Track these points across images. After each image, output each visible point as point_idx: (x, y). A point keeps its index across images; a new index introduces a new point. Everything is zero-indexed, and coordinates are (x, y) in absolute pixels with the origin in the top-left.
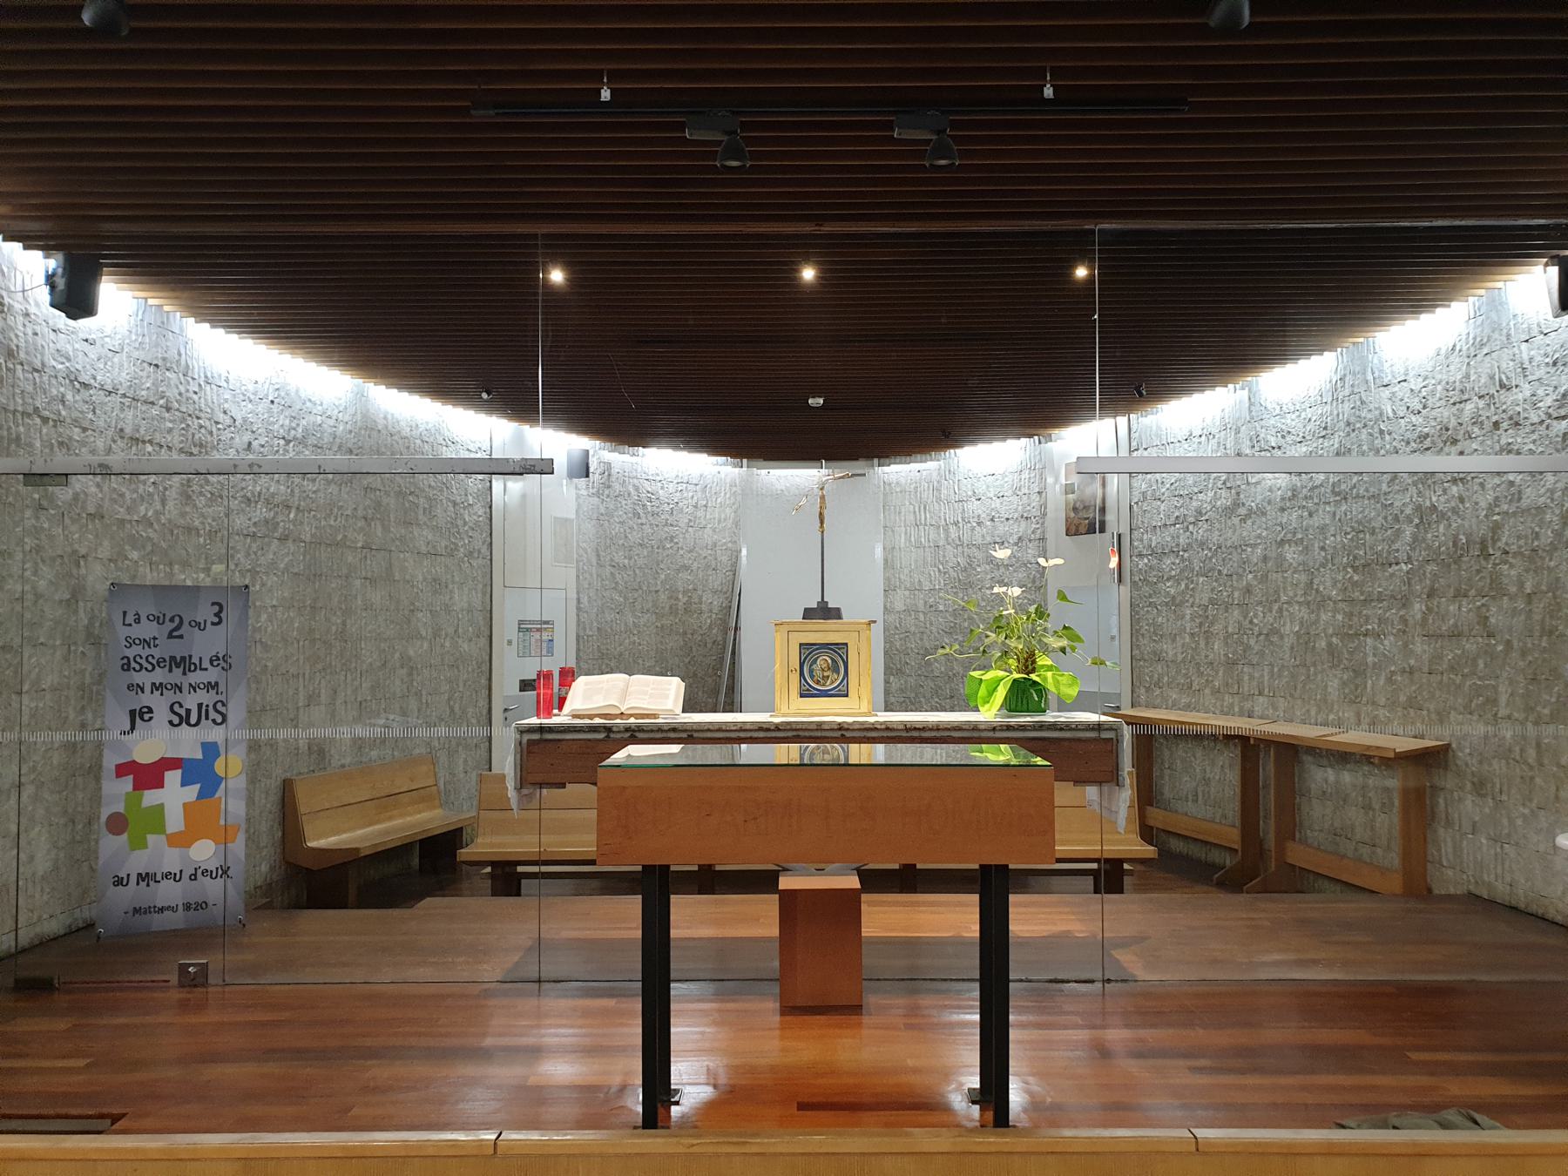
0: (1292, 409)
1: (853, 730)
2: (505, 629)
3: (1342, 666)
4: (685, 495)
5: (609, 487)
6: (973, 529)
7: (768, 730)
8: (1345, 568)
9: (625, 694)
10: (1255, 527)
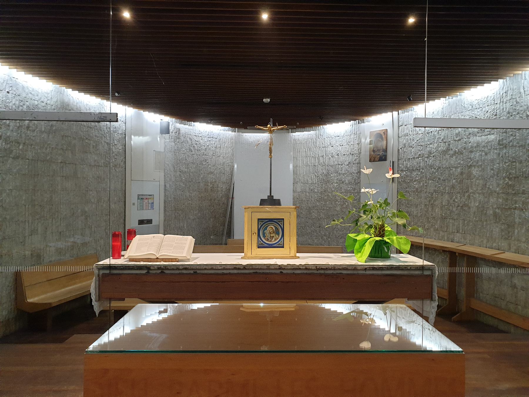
0: (478, 107)
2: (132, 198)
3: (501, 222)
4: (212, 142)
5: (179, 138)
6: (330, 158)
7: (239, 269)
8: (504, 178)
9: (160, 247)
10: (457, 159)
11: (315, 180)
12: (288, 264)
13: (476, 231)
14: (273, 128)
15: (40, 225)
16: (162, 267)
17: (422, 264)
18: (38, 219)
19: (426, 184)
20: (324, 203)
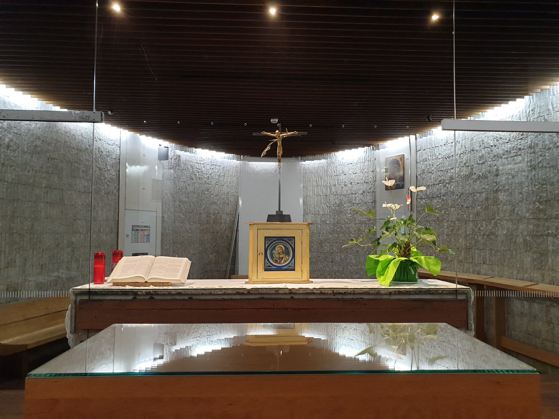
1: (299, 294)
2: (126, 229)
3: (532, 251)
5: (179, 165)
6: (342, 188)
7: (242, 294)
11: (327, 211)
12: (299, 288)
13: (504, 261)
14: (282, 135)
15: (18, 255)
16: (151, 292)
17: (456, 287)
18: (15, 249)
19: (448, 212)
20: (337, 236)
